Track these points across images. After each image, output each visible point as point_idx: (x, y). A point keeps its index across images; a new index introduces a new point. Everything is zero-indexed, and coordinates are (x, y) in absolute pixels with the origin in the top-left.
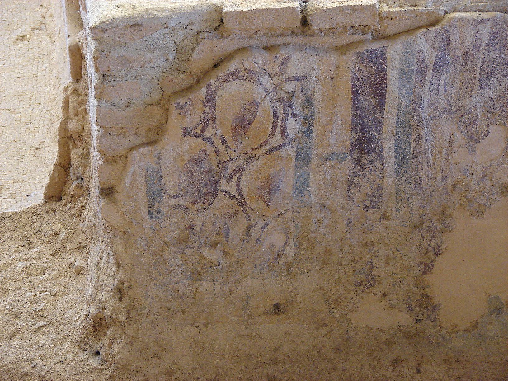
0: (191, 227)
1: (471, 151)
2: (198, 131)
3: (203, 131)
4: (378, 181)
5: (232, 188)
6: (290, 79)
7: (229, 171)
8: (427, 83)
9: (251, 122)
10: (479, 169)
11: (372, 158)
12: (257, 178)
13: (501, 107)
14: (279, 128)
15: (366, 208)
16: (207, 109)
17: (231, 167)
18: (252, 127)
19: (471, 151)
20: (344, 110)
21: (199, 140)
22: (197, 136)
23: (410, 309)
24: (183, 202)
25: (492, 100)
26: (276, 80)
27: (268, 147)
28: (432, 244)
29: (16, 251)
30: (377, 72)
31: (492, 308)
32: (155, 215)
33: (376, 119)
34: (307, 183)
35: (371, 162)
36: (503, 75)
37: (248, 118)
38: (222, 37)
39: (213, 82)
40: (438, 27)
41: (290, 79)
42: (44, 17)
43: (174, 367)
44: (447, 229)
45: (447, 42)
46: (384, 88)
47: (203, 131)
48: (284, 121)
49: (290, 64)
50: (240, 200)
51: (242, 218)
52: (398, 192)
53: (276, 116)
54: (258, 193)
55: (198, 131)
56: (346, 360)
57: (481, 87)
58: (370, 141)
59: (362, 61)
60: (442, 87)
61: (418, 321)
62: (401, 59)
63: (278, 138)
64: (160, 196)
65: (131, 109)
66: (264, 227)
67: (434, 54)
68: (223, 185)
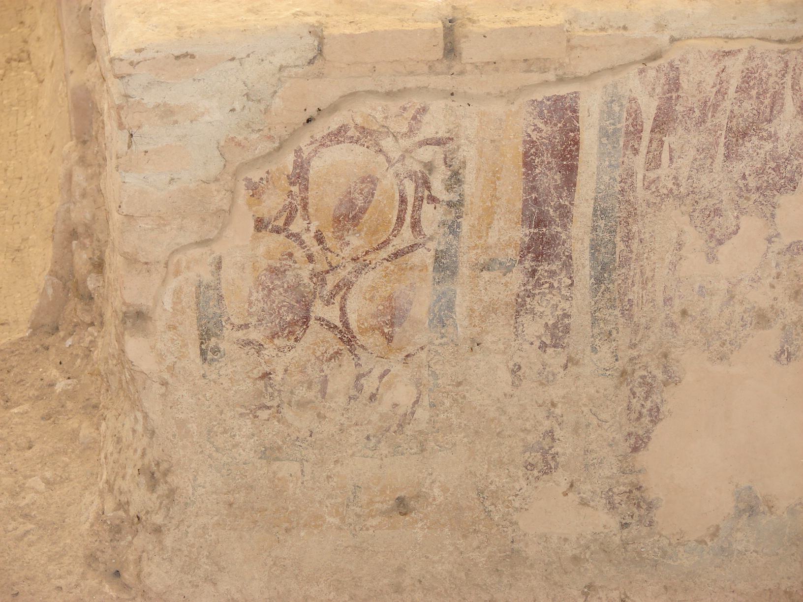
0: (266, 375)
1: (711, 257)
3: (287, 223)
5: (332, 314)
6: (427, 142)
7: (329, 287)
8: (643, 150)
9: (363, 210)
10: (723, 286)
11: (554, 268)
12: (371, 299)
13: (758, 189)
15: (543, 346)
16: (295, 189)
17: (331, 280)
19: (711, 257)
20: (512, 188)
21: (282, 237)
23: (612, 506)
24: (255, 335)
25: (744, 177)
26: (405, 143)
27: (390, 249)
28: (648, 404)
30: (565, 131)
31: (742, 506)
32: (210, 356)
33: (561, 206)
34: (450, 306)
35: (552, 273)
36: (762, 138)
37: (360, 203)
38: (320, 75)
39: (304, 143)
40: (661, 61)
41: (427, 142)
42: (25, 42)
44: (671, 380)
45: (674, 85)
46: (575, 158)
47: (287, 223)
48: (417, 208)
49: (426, 118)
52: (595, 321)
53: (403, 201)
54: (374, 322)
55: (280, 223)
57: (727, 157)
59: (541, 115)
61: (624, 526)
62: (602, 112)
63: (407, 235)
64: (219, 325)
65: (174, 187)
66: (382, 376)
68: (318, 309)
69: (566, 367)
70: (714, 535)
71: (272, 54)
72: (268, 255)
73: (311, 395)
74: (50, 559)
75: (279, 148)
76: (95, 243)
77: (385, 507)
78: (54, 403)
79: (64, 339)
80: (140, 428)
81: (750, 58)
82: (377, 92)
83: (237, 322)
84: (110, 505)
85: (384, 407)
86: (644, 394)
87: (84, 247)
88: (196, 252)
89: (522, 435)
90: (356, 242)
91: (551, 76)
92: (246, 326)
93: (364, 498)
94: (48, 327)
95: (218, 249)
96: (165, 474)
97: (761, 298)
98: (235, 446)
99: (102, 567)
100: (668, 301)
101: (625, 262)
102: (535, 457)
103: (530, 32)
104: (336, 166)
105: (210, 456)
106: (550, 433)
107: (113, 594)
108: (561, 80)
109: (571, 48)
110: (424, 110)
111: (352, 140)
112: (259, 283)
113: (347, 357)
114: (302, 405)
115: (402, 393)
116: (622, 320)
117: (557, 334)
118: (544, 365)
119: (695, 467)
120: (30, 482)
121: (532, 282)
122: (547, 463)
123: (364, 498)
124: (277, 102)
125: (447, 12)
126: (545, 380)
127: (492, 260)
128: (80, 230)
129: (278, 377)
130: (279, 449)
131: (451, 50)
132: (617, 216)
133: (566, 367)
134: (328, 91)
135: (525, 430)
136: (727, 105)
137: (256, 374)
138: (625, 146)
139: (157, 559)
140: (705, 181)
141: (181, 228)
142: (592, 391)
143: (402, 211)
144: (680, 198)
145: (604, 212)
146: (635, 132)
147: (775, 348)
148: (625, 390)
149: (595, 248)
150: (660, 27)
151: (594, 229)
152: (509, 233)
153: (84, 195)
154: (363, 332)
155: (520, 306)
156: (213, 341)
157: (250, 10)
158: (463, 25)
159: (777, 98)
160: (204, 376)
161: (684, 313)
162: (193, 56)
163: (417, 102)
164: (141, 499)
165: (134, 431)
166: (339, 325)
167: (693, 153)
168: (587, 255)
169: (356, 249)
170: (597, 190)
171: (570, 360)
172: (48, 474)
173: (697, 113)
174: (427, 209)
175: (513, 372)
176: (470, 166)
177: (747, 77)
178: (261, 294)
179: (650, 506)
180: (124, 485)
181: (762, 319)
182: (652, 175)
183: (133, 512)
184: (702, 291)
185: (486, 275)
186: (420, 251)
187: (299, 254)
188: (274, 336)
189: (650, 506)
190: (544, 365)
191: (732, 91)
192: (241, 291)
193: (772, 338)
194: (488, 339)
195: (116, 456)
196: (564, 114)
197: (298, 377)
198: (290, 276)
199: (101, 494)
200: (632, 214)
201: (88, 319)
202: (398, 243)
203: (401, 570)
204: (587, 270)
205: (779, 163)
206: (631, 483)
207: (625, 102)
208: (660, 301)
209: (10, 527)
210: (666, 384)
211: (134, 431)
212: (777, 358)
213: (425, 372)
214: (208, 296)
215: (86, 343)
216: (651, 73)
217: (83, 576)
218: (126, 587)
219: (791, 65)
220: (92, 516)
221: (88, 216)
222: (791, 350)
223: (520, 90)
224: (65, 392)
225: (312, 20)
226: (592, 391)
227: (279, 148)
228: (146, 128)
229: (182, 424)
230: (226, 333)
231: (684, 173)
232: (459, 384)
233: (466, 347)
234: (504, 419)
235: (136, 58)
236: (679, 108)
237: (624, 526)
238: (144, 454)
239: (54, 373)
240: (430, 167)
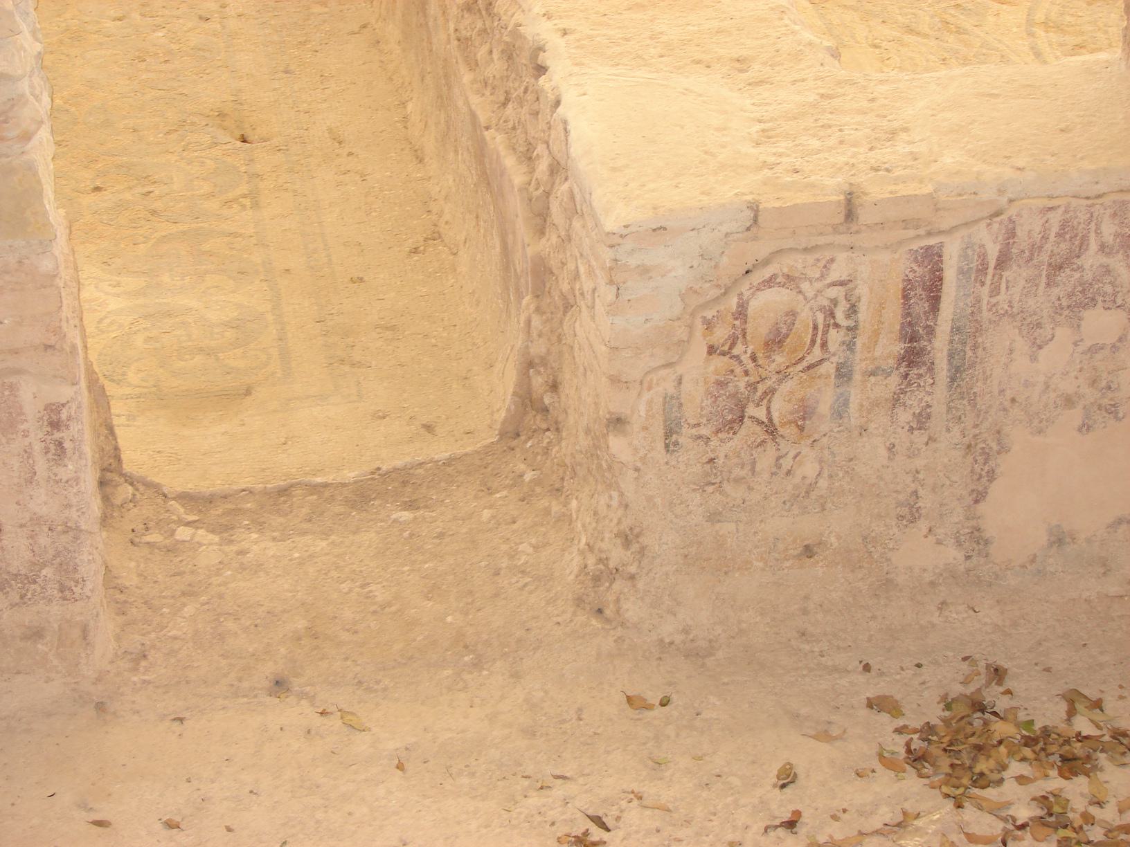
0: (711, 460)
1: (1034, 359)
2: (726, 348)
3: (730, 348)
4: (928, 399)
5: (761, 413)
6: (834, 284)
7: (759, 393)
8: (988, 282)
9: (787, 336)
10: (1042, 379)
11: (921, 371)
12: (789, 401)
13: (1069, 307)
14: (819, 341)
15: (911, 429)
16: (737, 323)
17: (761, 388)
18: (788, 340)
19: (1034, 359)
20: (893, 315)
21: (726, 359)
22: (723, 354)
23: (959, 544)
24: (704, 431)
25: (1059, 299)
26: (818, 285)
27: (805, 364)
28: (986, 468)
29: (476, 497)
30: (932, 271)
31: (1053, 539)
32: (672, 448)
33: (928, 326)
34: (846, 403)
35: (920, 376)
36: (1073, 270)
37: (784, 331)
38: (755, 239)
39: (745, 288)
40: (1002, 217)
41: (834, 284)
42: (435, 225)
43: (690, 623)
44: (1003, 449)
45: (1012, 234)
46: (939, 290)
47: (730, 348)
48: (825, 332)
49: (834, 266)
50: (771, 429)
51: (770, 445)
52: (949, 409)
53: (815, 328)
54: (790, 418)
55: (726, 348)
56: (886, 605)
57: (1048, 285)
58: (921, 352)
59: (916, 260)
60: (1003, 286)
61: (968, 557)
62: (960, 256)
63: (817, 353)
64: (679, 425)
65: (648, 325)
66: (795, 457)
67: (998, 247)
68: (751, 410)
69: (927, 444)
70: (1033, 561)
71: (721, 224)
72: (716, 372)
73: (742, 473)
74: (548, 603)
75: (725, 294)
76: (549, 371)
77: (796, 552)
78: (525, 489)
79: (526, 442)
80: (615, 503)
81: (1066, 212)
82: (796, 249)
83: (692, 422)
84: (591, 561)
85: (797, 480)
86: (983, 463)
87: (539, 373)
88: (663, 372)
89: (895, 495)
90: (780, 359)
91: (922, 232)
92: (699, 425)
93: (781, 546)
94: (512, 433)
95: (680, 370)
96: (637, 536)
97: (1068, 386)
98: (690, 513)
99: (588, 607)
100: (1002, 392)
101: (973, 365)
102: (905, 511)
103: (908, 199)
104: (767, 305)
105: (671, 522)
106: (915, 493)
107: (600, 626)
108: (929, 234)
109: (937, 210)
110: (832, 260)
111: (780, 285)
112: (709, 393)
113: (770, 444)
114: (738, 481)
115: (809, 469)
116: (969, 408)
117: (922, 420)
118: (912, 443)
119: (1017, 514)
120: (521, 548)
121: (905, 382)
122: (912, 514)
123: (781, 546)
124: (725, 260)
125: (846, 188)
126: (912, 455)
127: (877, 368)
128: (537, 361)
129: (720, 461)
130: (720, 513)
131: (850, 215)
132: (969, 332)
133: (927, 444)
134: (762, 249)
135: (897, 492)
136: (1048, 247)
137: (705, 459)
138: (976, 280)
139: (632, 599)
140: (1031, 303)
141: (652, 355)
142: (946, 460)
143: (815, 335)
144: (1013, 316)
145: (958, 329)
146: (983, 270)
147: (1078, 422)
148: (970, 459)
149: (951, 356)
150: (1001, 192)
151: (951, 342)
152: (890, 347)
153: (540, 336)
154: (783, 425)
155: (896, 401)
156: (674, 436)
157: (703, 193)
158: (859, 197)
159: (1085, 239)
160: (667, 463)
161: (1013, 400)
162: (665, 229)
163: (828, 255)
164: (617, 555)
165: (609, 506)
166: (766, 421)
167: (1023, 283)
168: (945, 361)
169: (779, 365)
170: (955, 313)
171: (930, 438)
172: (533, 541)
173: (1027, 254)
174: (833, 332)
175: (889, 449)
176: (864, 299)
177: (1064, 225)
178: (710, 401)
179: (987, 542)
180: (604, 546)
181: (1069, 402)
182: (994, 300)
183: (612, 565)
184: (1027, 384)
185: (872, 379)
186: (826, 364)
187: (739, 370)
188: (718, 431)
189: (987, 542)
190: (912, 443)
191: (1052, 238)
192: (695, 397)
193: (1075, 416)
194: (872, 426)
195: (594, 525)
196: (932, 258)
197: (736, 460)
198: (731, 388)
199: (581, 552)
200: (979, 330)
201: (544, 426)
202: (811, 359)
203: (807, 598)
204: (945, 373)
205: (1084, 287)
206: (973, 527)
207: (976, 248)
208: (996, 392)
209: (513, 581)
210: (999, 453)
211: (609, 506)
212: (1080, 430)
213: (826, 452)
214: (672, 403)
215: (544, 444)
216: (996, 226)
217: (574, 614)
218: (608, 621)
219: (1095, 215)
220: (576, 570)
221: (544, 350)
222: (1090, 423)
223: (901, 243)
224: (531, 481)
225: (749, 198)
226: (946, 460)
227: (725, 294)
228: (629, 284)
229: (650, 499)
230: (684, 430)
231: (1017, 298)
232: (851, 460)
233: (856, 433)
234: (882, 483)
235: (625, 232)
236: (1014, 251)
237: (968, 557)
238: (619, 522)
239: (522, 467)
240: (835, 302)
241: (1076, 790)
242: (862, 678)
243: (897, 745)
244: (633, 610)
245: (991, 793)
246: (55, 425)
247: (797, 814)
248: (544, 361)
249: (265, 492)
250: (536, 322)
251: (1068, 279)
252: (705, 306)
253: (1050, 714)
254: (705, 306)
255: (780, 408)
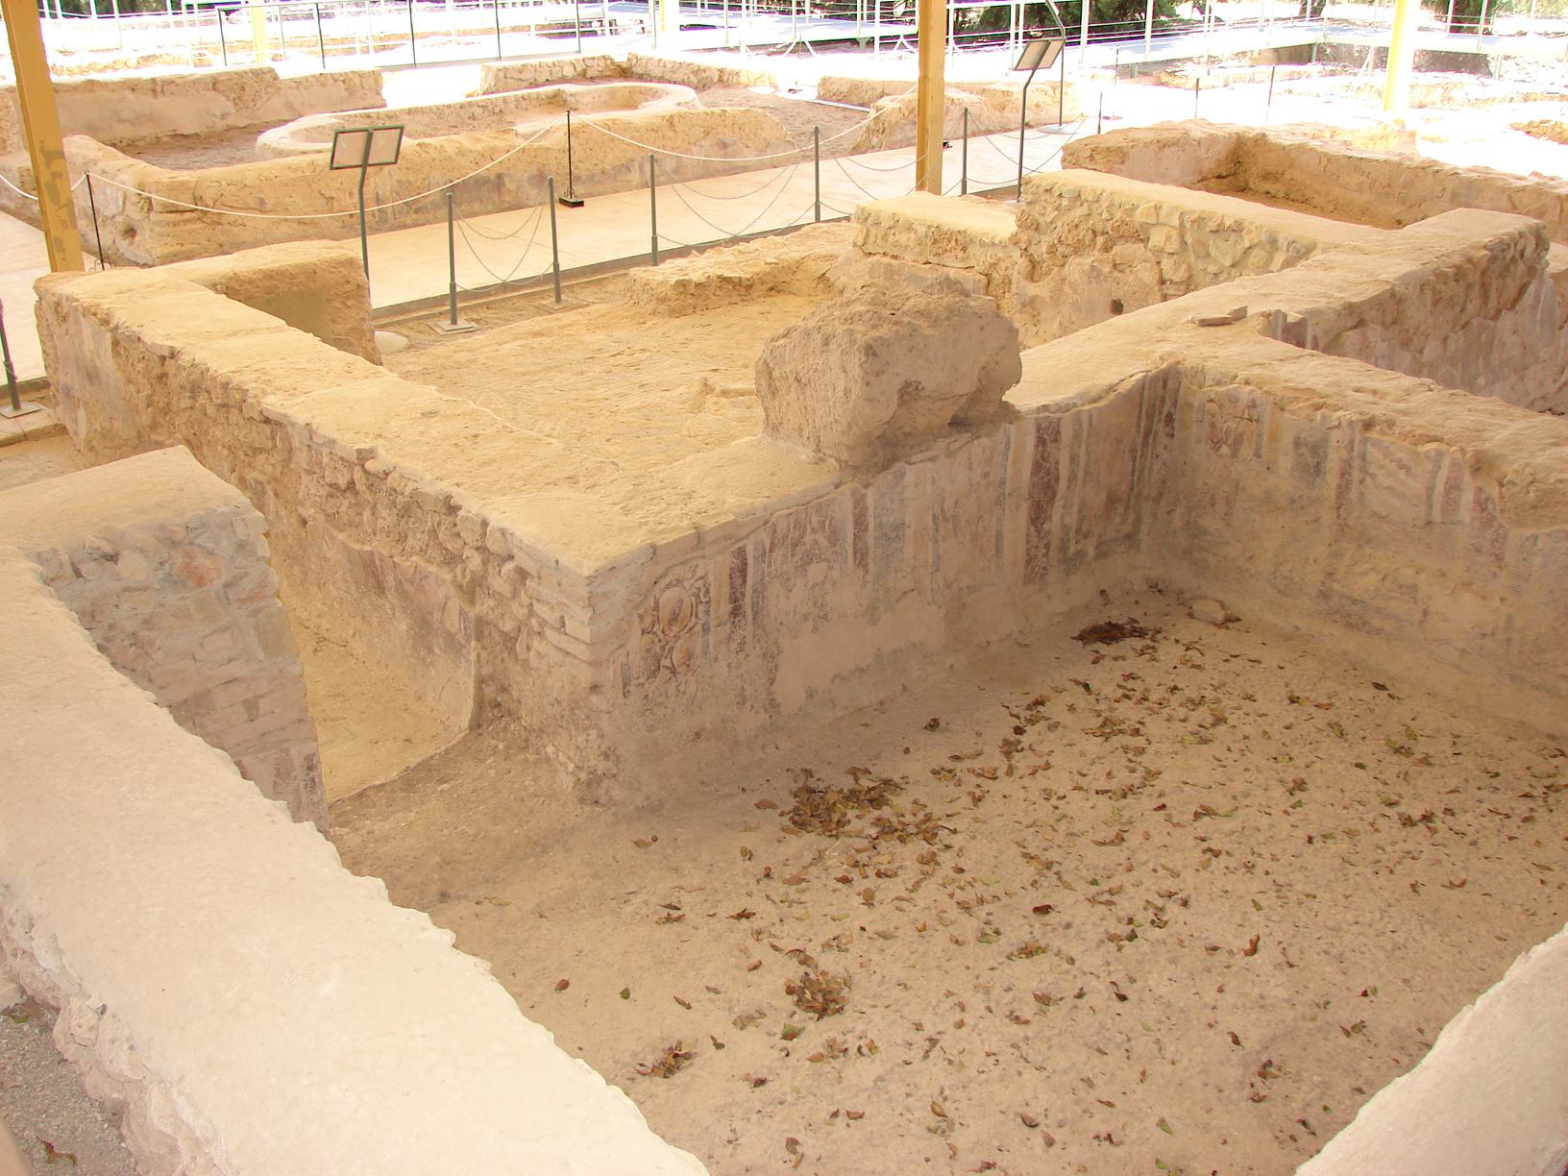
20: (726, 590)
94: (476, 725)
104: (668, 598)
117: (742, 645)
119: (790, 688)
132: (759, 592)
134: (660, 569)
155: (730, 638)
164: (602, 766)
181: (806, 618)
193: (810, 625)
196: (741, 553)
214: (626, 668)
241: (886, 812)
242: (744, 796)
243: (786, 821)
244: (618, 794)
245: (847, 828)
246: (310, 768)
247: (768, 869)
248: (492, 677)
249: (351, 798)
250: (484, 654)
251: (800, 550)
252: (637, 606)
253: (848, 784)
254: (637, 606)
255: (676, 656)
